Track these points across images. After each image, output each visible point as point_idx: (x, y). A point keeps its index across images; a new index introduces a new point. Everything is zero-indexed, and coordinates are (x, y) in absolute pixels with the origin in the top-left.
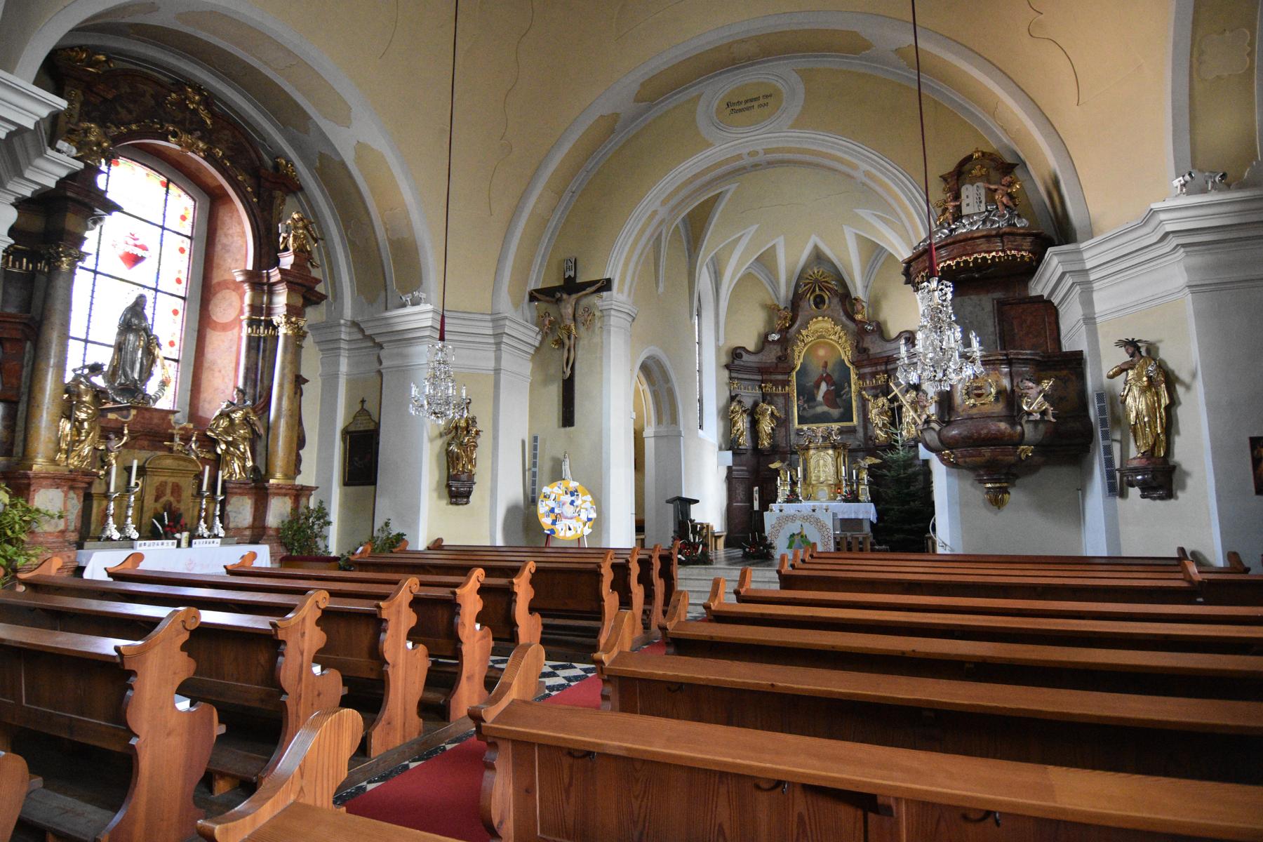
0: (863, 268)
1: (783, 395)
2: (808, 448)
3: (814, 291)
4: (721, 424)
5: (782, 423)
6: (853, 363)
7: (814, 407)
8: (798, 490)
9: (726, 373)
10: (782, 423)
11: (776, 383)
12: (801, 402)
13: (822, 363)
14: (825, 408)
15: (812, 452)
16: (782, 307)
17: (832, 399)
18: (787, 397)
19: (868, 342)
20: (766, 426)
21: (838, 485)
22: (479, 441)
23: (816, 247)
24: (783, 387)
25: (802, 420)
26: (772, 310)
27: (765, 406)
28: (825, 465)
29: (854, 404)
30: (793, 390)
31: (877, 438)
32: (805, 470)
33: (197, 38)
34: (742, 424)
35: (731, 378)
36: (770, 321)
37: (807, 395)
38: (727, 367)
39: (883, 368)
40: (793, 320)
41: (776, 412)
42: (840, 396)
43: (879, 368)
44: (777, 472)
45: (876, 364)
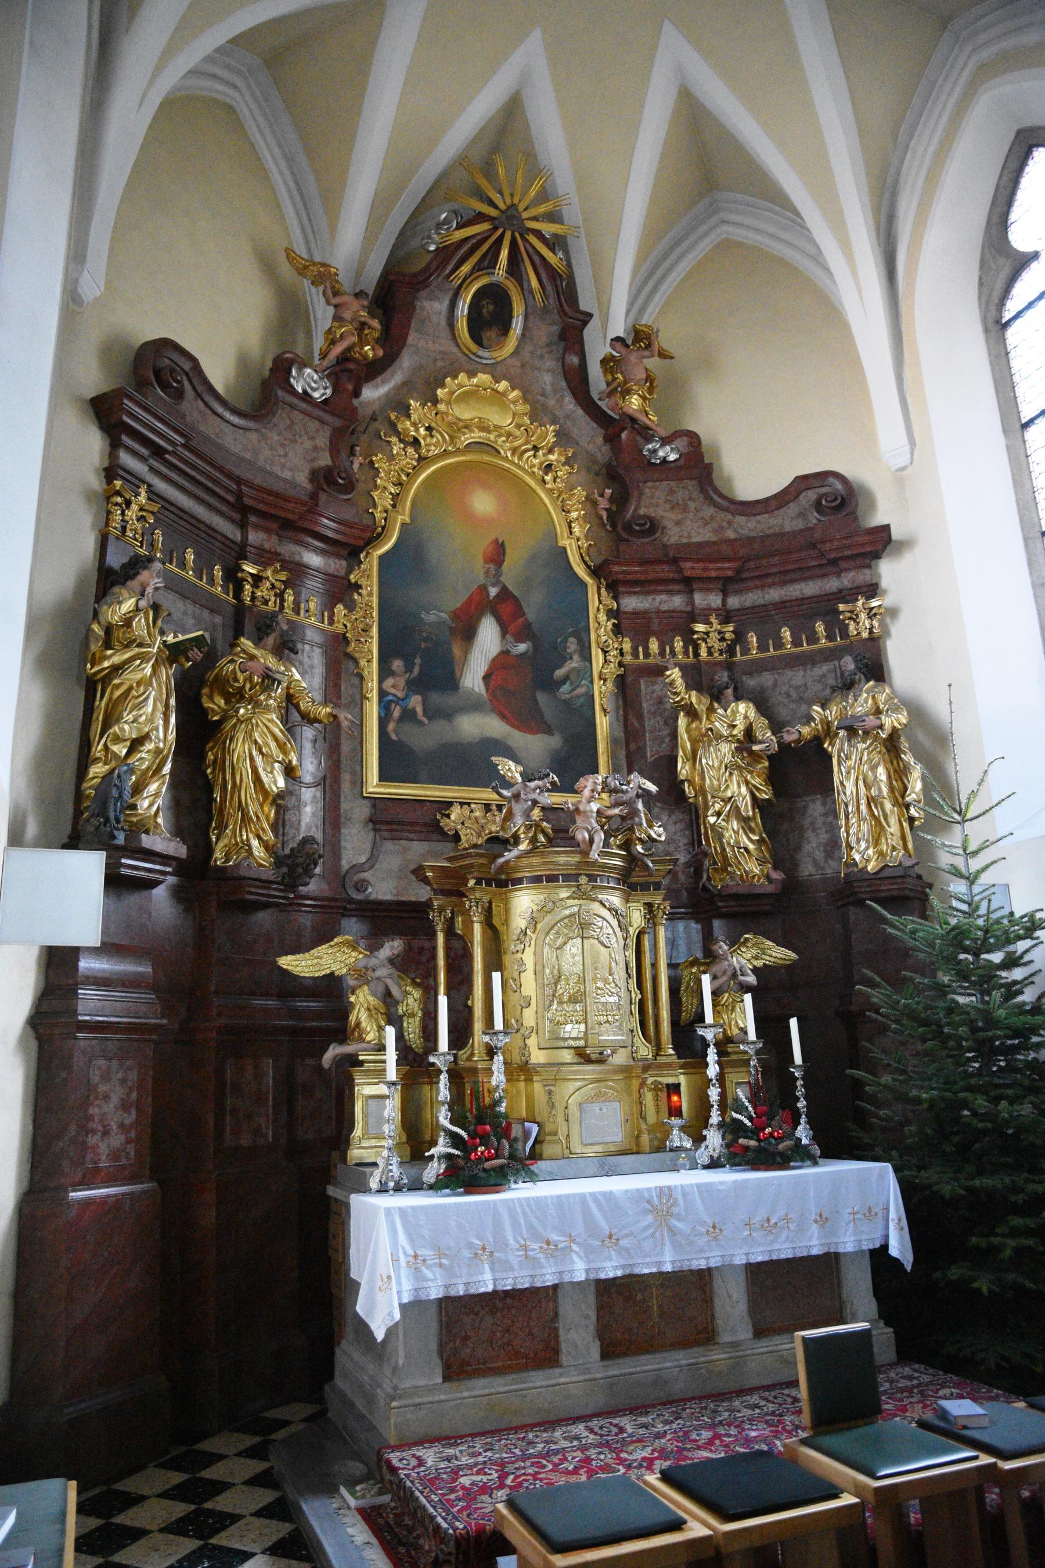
0: (651, 235)
3: (489, 262)
4: (37, 695)
6: (596, 572)
7: (448, 715)
9: (93, 443)
12: (396, 686)
13: (483, 544)
14: (493, 726)
15: (524, 902)
16: (345, 280)
19: (653, 501)
22: (682, 1171)
23: (512, 112)
25: (396, 762)
26: (295, 277)
29: (603, 724)
33: (306, 1519)
34: (150, 717)
35: (110, 472)
36: (290, 313)
37: (423, 657)
38: (104, 411)
40: (392, 343)
42: (551, 685)
43: (700, 599)
44: (331, 990)
45: (688, 584)
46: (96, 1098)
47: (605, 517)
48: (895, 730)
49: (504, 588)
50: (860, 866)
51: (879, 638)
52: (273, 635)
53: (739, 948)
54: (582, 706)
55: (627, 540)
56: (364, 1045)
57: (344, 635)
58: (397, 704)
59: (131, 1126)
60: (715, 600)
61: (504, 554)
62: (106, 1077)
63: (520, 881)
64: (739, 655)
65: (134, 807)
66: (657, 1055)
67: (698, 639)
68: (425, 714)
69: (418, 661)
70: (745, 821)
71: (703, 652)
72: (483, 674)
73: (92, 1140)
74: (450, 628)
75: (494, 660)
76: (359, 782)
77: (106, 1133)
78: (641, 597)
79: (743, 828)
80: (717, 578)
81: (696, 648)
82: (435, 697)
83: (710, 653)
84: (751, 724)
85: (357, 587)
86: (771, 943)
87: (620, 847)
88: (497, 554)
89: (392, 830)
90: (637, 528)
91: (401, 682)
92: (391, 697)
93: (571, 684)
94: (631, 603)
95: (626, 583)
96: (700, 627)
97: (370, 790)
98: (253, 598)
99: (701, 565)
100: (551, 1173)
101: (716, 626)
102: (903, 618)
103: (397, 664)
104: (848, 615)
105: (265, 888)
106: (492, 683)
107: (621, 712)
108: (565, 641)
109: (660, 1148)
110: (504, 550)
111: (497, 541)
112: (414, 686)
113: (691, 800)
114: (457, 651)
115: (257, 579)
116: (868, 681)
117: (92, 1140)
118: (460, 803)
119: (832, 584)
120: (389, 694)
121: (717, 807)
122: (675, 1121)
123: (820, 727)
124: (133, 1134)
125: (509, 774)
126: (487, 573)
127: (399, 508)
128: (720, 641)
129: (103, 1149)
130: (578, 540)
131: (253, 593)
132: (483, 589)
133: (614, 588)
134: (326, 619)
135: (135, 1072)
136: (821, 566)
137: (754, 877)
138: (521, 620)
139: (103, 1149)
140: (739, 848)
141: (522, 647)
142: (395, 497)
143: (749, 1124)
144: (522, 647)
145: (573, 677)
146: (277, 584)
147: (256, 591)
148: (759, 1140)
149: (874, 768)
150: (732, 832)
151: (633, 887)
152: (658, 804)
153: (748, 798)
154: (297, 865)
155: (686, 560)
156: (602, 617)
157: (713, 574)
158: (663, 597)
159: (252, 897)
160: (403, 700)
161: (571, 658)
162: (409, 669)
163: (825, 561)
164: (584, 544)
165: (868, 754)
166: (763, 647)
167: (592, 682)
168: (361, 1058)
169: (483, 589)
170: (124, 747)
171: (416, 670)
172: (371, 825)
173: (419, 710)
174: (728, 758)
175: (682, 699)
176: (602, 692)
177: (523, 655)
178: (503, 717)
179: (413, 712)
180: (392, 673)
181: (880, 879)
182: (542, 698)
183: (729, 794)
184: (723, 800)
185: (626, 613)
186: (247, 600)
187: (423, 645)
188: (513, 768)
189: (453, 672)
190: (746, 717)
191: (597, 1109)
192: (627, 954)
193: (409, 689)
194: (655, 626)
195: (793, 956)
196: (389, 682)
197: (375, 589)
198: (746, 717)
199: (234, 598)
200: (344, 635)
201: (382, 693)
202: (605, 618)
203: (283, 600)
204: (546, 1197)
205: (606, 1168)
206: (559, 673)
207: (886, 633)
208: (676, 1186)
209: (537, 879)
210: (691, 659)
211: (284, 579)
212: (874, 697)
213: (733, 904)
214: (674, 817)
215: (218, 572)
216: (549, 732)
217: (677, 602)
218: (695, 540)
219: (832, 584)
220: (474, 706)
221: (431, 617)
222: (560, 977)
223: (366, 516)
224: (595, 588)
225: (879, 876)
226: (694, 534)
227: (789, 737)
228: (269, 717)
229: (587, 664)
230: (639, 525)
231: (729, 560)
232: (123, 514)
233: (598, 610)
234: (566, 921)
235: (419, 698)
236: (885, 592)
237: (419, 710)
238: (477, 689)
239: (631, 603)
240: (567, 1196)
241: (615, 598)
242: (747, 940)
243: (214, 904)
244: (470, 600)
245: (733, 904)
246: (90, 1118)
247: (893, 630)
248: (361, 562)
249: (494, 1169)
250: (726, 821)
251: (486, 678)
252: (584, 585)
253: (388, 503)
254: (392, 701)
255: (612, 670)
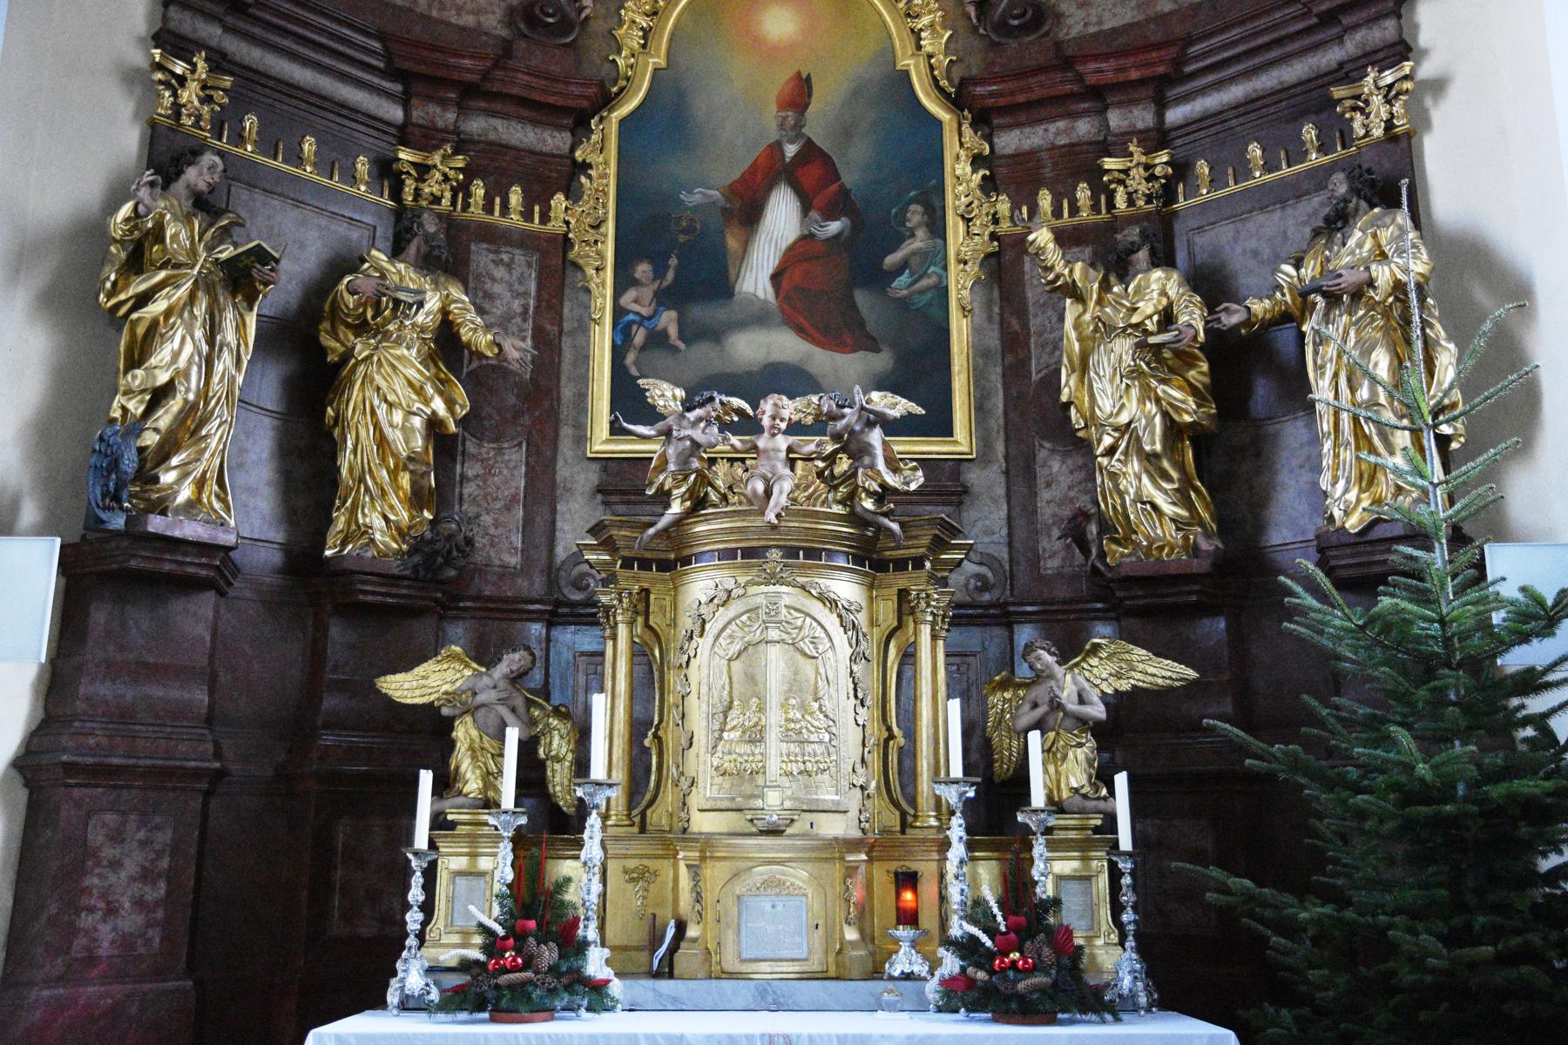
1: (527, 241)
2: (673, 557)
5: (509, 403)
6: (956, 102)
7: (715, 334)
8: (580, 876)
10: (509, 403)
11: (493, 166)
12: (638, 301)
13: (778, 81)
14: (785, 345)
15: (701, 585)
17: (829, 292)
18: (556, 262)
20: (395, 401)
21: (890, 849)
24: (538, 197)
27: (403, 273)
28: (803, 694)
29: (960, 330)
30: (592, 219)
31: (1115, 528)
32: (644, 736)
37: (681, 259)
39: (1143, 117)
41: (475, 333)
42: (879, 279)
43: (1116, 119)
44: (430, 732)
45: (1099, 96)
46: (98, 864)
47: (973, 15)
48: (1399, 287)
49: (809, 142)
50: (1338, 523)
51: (1409, 135)
52: (415, 242)
53: (1084, 660)
54: (930, 304)
55: (999, 44)
56: (460, 800)
57: (566, 235)
58: (640, 324)
59: (157, 904)
60: (1143, 117)
61: (810, 95)
62: (116, 837)
63: (699, 557)
64: (1181, 198)
65: (156, 480)
66: (904, 825)
67: (1111, 182)
68: (681, 337)
69: (673, 262)
70: (1150, 459)
71: (1121, 202)
72: (771, 271)
73: (86, 921)
74: (724, 210)
75: (791, 248)
76: (581, 439)
77: (112, 911)
78: (1027, 130)
79: (1147, 472)
80: (1142, 82)
81: (1111, 196)
82: (701, 313)
83: (1131, 202)
84: (1170, 305)
85: (585, 166)
86: (1144, 652)
87: (842, 502)
88: (800, 94)
89: (628, 503)
90: (1016, 22)
91: (647, 293)
92: (631, 317)
93: (912, 275)
94: (1010, 141)
95: (1001, 111)
96: (1110, 163)
97: (597, 448)
98: (417, 193)
99: (1112, 63)
100: (675, 999)
101: (1139, 157)
102: (1454, 93)
103: (643, 270)
104: (1348, 103)
105: (392, 585)
106: (785, 285)
107: (996, 310)
108: (904, 210)
109: (876, 972)
110: (810, 87)
111: (799, 73)
112: (664, 298)
113: (1080, 434)
114: (732, 243)
115: (423, 170)
116: (1372, 206)
117: (86, 921)
118: (729, 459)
119: (1331, 57)
120: (629, 312)
121: (1107, 441)
122: (904, 932)
123: (1288, 298)
124: (160, 914)
125: (661, 403)
126: (782, 126)
127: (652, 44)
128: (1148, 180)
129: (106, 934)
130: (930, 56)
131: (416, 189)
132: (777, 147)
133: (983, 121)
134: (497, 208)
135: (169, 833)
136: (1308, 30)
137: (1161, 548)
138: (834, 187)
139: (106, 934)
140: (1143, 503)
141: (834, 227)
142: (646, 33)
143: (989, 943)
144: (834, 227)
145: (914, 262)
146: (452, 174)
147: (421, 186)
148: (992, 972)
149: (1367, 352)
150: (1134, 481)
151: (880, 566)
152: (1047, 445)
153: (1158, 420)
154: (437, 552)
155: (1086, 58)
156: (964, 168)
157: (1134, 75)
158: (1061, 124)
159: (370, 598)
160: (650, 318)
161: (913, 235)
162: (659, 273)
163: (1315, 20)
164: (942, 61)
165: (1358, 332)
166: (1216, 182)
167: (945, 268)
168: (450, 817)
169: (777, 147)
170: (141, 402)
171: (670, 276)
172: (599, 497)
173: (673, 331)
174: (1128, 360)
175: (1058, 277)
176: (961, 283)
177: (837, 236)
178: (800, 331)
179: (664, 334)
180: (635, 283)
181: (1372, 542)
182: (862, 298)
183: (1124, 418)
184: (1116, 429)
185: (1003, 156)
186: (408, 199)
187: (682, 238)
188: (669, 394)
189: (726, 271)
190: (1163, 293)
191: (768, 907)
192: (855, 668)
193: (659, 304)
194: (1047, 172)
195: (1191, 674)
196: (627, 299)
197: (612, 170)
198: (1163, 293)
199: (391, 198)
200: (566, 235)
201: (619, 312)
202: (969, 169)
203: (468, 195)
204: (570, 1036)
205: (770, 999)
206: (891, 260)
207: (1422, 121)
208: (798, 1036)
209: (729, 554)
210: (1104, 214)
211: (461, 165)
212: (1375, 236)
213: (1139, 593)
214: (1070, 462)
215: (362, 165)
216: (872, 345)
217: (1084, 128)
218: (1106, 26)
219: (1331, 57)
220: (758, 318)
221: (694, 198)
222: (731, 702)
223: (607, 66)
224: (955, 126)
225: (1368, 538)
226: (1106, 15)
227: (1232, 318)
228: (398, 352)
229: (939, 241)
230: (1015, 17)
231: (1158, 46)
232: (175, 95)
233: (958, 157)
234: (744, 618)
235: (673, 314)
236: (1424, 53)
237: (673, 331)
238: (761, 294)
239: (1010, 141)
240: (415, 1035)
241: (989, 138)
242: (1096, 647)
243: (329, 607)
244: (754, 167)
245: (1139, 593)
246: (87, 891)
247: (1437, 116)
248: (592, 131)
249: (511, 987)
250: (1125, 463)
251: (776, 278)
252: (939, 123)
253: (635, 41)
254: (633, 322)
255: (983, 243)
